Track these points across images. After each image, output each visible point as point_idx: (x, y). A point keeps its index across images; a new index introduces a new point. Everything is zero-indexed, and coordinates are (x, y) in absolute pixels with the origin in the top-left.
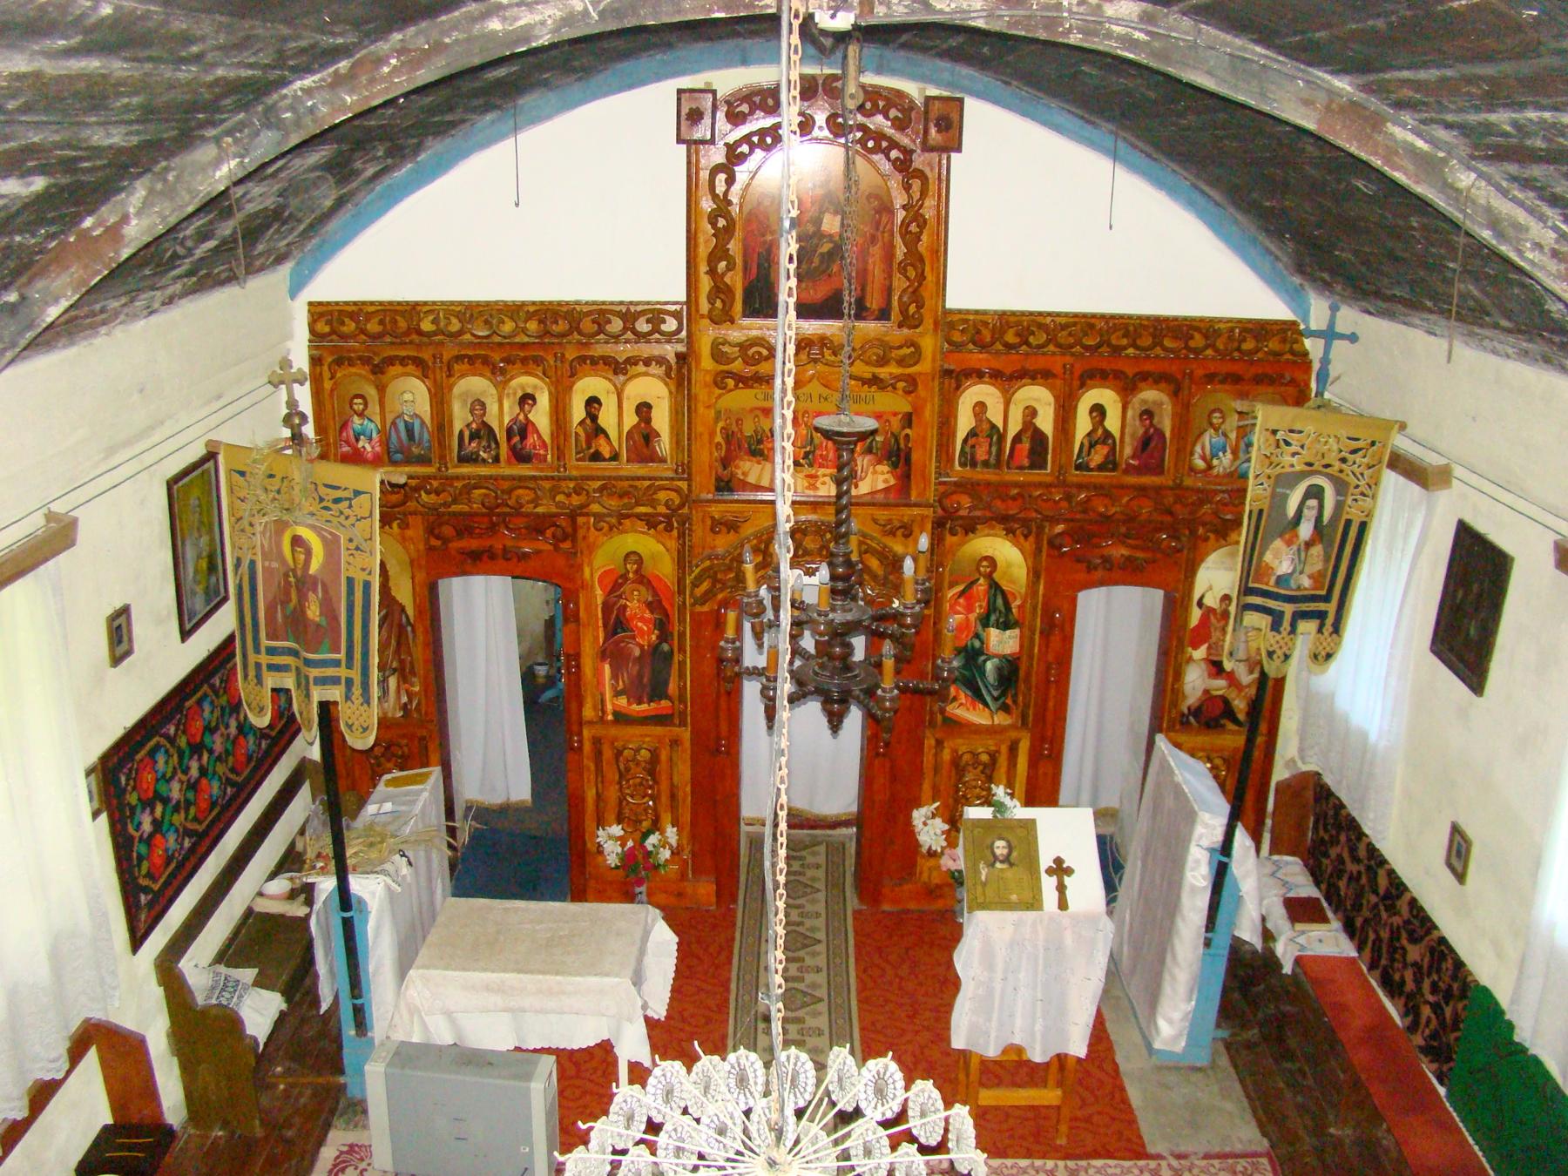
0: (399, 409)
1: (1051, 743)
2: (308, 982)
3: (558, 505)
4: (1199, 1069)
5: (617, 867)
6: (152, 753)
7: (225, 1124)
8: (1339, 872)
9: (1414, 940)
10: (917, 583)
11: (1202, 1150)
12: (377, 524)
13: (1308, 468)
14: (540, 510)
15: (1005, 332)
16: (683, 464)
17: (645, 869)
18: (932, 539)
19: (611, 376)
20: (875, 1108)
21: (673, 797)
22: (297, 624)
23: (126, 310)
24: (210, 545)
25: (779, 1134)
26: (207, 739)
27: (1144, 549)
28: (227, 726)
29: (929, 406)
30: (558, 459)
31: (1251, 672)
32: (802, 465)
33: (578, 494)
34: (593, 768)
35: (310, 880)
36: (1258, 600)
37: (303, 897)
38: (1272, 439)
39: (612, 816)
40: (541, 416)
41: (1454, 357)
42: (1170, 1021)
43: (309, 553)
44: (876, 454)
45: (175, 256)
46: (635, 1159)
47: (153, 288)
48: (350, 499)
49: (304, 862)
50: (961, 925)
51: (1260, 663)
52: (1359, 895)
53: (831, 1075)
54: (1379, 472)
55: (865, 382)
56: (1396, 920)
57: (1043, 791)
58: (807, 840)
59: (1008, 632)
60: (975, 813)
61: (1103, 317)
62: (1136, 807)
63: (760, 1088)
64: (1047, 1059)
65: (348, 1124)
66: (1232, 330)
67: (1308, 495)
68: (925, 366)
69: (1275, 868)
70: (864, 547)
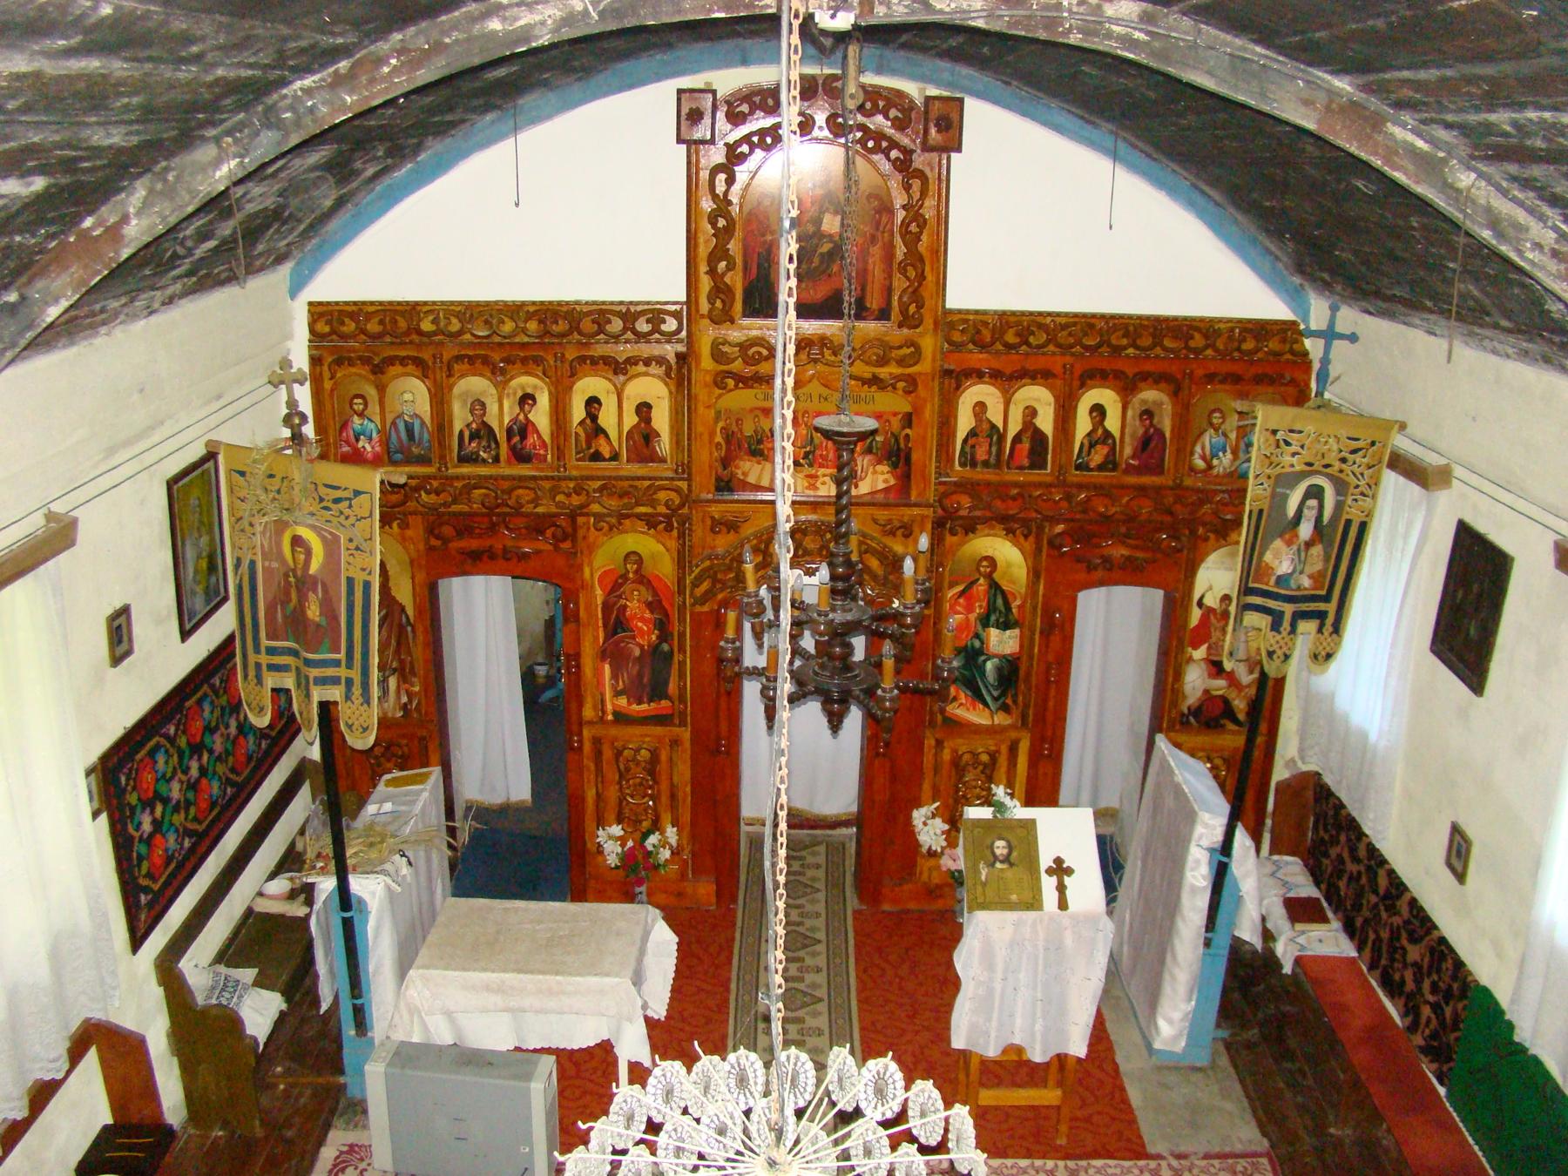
0: (399, 409)
2: (308, 982)
3: (558, 505)
4: (1199, 1069)
5: (617, 867)
6: (152, 753)
7: (225, 1124)
8: (1339, 872)
9: (1414, 940)
10: (917, 583)
11: (1202, 1150)
13: (1308, 468)
14: (540, 510)
16: (683, 464)
17: (645, 869)
18: (932, 539)
19: (611, 376)
20: (875, 1108)
21: (673, 796)
22: (297, 624)
23: (126, 310)
25: (779, 1134)
26: (208, 740)
28: (227, 726)
29: (929, 406)
30: (558, 459)
31: (1251, 672)
32: (802, 465)
35: (310, 880)
37: (303, 896)
38: (1272, 439)
40: (541, 416)
42: (1170, 1021)
43: (309, 553)
44: (876, 454)
45: (175, 256)
46: (635, 1159)
47: (153, 289)
48: (350, 499)
49: (304, 862)
50: (961, 925)
51: (1260, 663)
52: (1359, 895)
53: (832, 1075)
54: (1379, 472)
56: (1396, 920)
57: (1043, 791)
58: (807, 840)
59: (1008, 632)
60: (976, 813)
61: (1103, 317)
62: (1136, 807)
63: (760, 1088)
65: (347, 1124)
66: (1232, 330)
67: (1308, 495)
68: (924, 367)
69: (1275, 868)
70: (864, 547)
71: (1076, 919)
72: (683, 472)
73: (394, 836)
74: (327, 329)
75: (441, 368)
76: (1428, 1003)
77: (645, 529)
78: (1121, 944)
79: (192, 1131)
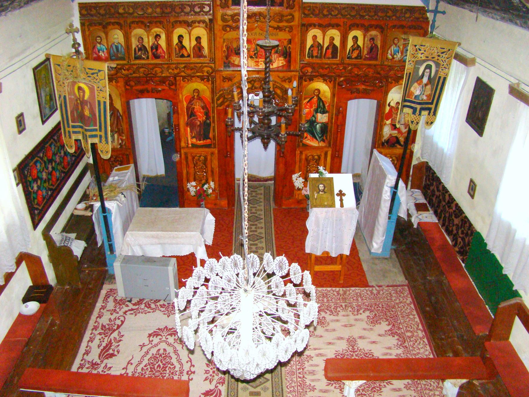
1: (339, 151)
2: (93, 237)
3: (169, 73)
4: (386, 259)
5: (194, 196)
6: (35, 163)
7: (69, 284)
8: (433, 195)
9: (456, 217)
10: (293, 98)
11: (387, 284)
12: (107, 82)
13: (427, 59)
14: (163, 75)
15: (323, 10)
16: (212, 58)
17: (204, 196)
18: (298, 83)
19: (187, 28)
20: (279, 272)
21: (212, 171)
22: (82, 117)
23: (11, 6)
24: (50, 91)
25: (247, 281)
26: (54, 158)
27: (370, 86)
28: (60, 153)
29: (297, 37)
30: (169, 57)
31: (406, 128)
33: (177, 69)
34: (185, 163)
35: (92, 203)
36: (408, 104)
37: (90, 209)
38: (414, 48)
39: (192, 178)
40: (163, 42)
41: (478, 19)
42: (377, 243)
43: (84, 92)
44: (279, 54)
46: (201, 290)
48: (97, 73)
49: (89, 198)
50: (308, 213)
51: (409, 125)
52: (440, 202)
53: (265, 262)
54: (451, 60)
55: (275, 28)
56: (451, 211)
57: (336, 168)
58: (258, 186)
61: (357, 5)
62: (367, 172)
63: (242, 267)
64: (336, 256)
65: (109, 282)
66: (402, 10)
67: (426, 68)
68: (295, 23)
69: (412, 193)
70: (275, 86)
71: (347, 210)
72: (213, 61)
73: (119, 188)
74: (86, 13)
75: (127, 26)
76: (460, 237)
77: (200, 81)
78: (361, 218)
79: (59, 287)
